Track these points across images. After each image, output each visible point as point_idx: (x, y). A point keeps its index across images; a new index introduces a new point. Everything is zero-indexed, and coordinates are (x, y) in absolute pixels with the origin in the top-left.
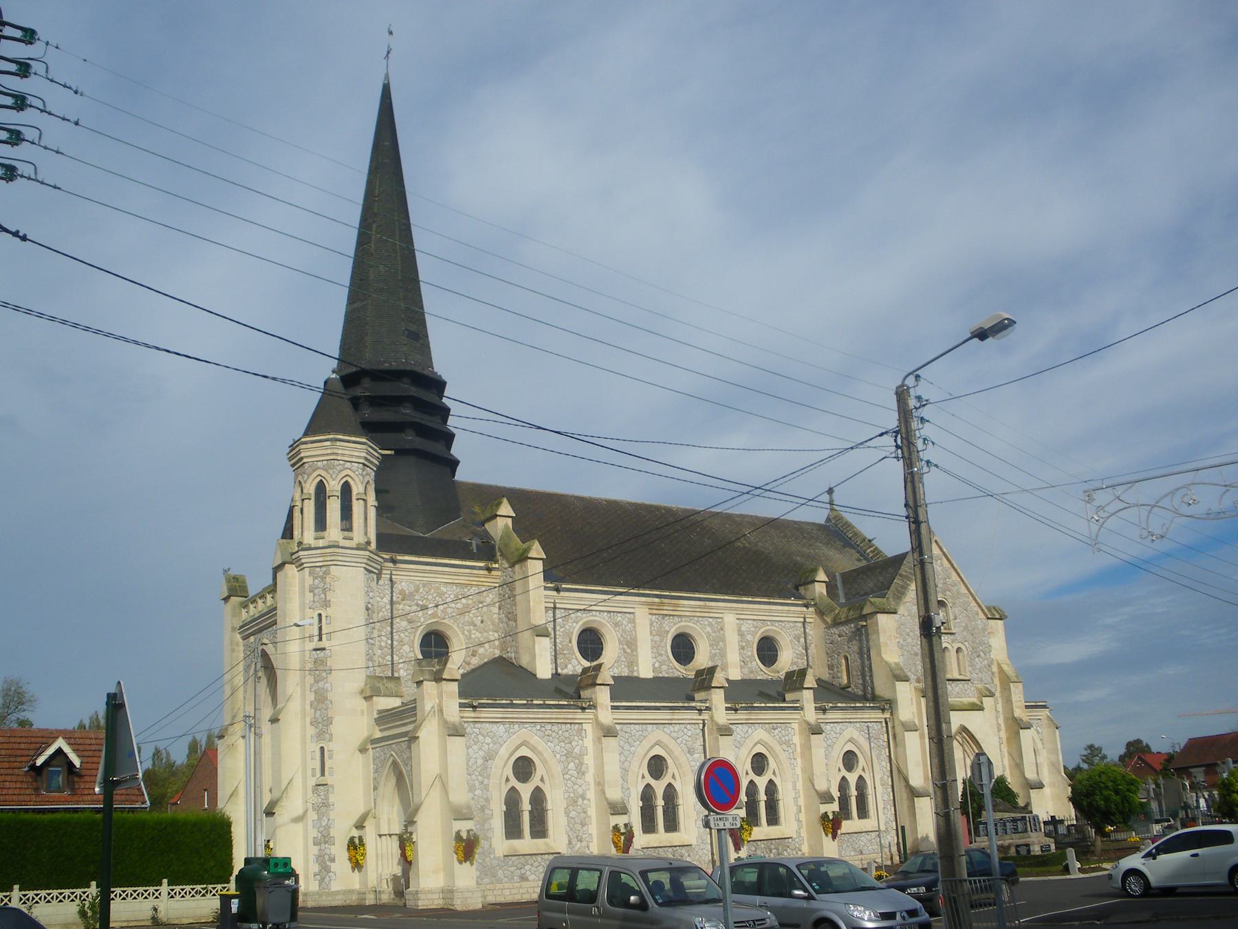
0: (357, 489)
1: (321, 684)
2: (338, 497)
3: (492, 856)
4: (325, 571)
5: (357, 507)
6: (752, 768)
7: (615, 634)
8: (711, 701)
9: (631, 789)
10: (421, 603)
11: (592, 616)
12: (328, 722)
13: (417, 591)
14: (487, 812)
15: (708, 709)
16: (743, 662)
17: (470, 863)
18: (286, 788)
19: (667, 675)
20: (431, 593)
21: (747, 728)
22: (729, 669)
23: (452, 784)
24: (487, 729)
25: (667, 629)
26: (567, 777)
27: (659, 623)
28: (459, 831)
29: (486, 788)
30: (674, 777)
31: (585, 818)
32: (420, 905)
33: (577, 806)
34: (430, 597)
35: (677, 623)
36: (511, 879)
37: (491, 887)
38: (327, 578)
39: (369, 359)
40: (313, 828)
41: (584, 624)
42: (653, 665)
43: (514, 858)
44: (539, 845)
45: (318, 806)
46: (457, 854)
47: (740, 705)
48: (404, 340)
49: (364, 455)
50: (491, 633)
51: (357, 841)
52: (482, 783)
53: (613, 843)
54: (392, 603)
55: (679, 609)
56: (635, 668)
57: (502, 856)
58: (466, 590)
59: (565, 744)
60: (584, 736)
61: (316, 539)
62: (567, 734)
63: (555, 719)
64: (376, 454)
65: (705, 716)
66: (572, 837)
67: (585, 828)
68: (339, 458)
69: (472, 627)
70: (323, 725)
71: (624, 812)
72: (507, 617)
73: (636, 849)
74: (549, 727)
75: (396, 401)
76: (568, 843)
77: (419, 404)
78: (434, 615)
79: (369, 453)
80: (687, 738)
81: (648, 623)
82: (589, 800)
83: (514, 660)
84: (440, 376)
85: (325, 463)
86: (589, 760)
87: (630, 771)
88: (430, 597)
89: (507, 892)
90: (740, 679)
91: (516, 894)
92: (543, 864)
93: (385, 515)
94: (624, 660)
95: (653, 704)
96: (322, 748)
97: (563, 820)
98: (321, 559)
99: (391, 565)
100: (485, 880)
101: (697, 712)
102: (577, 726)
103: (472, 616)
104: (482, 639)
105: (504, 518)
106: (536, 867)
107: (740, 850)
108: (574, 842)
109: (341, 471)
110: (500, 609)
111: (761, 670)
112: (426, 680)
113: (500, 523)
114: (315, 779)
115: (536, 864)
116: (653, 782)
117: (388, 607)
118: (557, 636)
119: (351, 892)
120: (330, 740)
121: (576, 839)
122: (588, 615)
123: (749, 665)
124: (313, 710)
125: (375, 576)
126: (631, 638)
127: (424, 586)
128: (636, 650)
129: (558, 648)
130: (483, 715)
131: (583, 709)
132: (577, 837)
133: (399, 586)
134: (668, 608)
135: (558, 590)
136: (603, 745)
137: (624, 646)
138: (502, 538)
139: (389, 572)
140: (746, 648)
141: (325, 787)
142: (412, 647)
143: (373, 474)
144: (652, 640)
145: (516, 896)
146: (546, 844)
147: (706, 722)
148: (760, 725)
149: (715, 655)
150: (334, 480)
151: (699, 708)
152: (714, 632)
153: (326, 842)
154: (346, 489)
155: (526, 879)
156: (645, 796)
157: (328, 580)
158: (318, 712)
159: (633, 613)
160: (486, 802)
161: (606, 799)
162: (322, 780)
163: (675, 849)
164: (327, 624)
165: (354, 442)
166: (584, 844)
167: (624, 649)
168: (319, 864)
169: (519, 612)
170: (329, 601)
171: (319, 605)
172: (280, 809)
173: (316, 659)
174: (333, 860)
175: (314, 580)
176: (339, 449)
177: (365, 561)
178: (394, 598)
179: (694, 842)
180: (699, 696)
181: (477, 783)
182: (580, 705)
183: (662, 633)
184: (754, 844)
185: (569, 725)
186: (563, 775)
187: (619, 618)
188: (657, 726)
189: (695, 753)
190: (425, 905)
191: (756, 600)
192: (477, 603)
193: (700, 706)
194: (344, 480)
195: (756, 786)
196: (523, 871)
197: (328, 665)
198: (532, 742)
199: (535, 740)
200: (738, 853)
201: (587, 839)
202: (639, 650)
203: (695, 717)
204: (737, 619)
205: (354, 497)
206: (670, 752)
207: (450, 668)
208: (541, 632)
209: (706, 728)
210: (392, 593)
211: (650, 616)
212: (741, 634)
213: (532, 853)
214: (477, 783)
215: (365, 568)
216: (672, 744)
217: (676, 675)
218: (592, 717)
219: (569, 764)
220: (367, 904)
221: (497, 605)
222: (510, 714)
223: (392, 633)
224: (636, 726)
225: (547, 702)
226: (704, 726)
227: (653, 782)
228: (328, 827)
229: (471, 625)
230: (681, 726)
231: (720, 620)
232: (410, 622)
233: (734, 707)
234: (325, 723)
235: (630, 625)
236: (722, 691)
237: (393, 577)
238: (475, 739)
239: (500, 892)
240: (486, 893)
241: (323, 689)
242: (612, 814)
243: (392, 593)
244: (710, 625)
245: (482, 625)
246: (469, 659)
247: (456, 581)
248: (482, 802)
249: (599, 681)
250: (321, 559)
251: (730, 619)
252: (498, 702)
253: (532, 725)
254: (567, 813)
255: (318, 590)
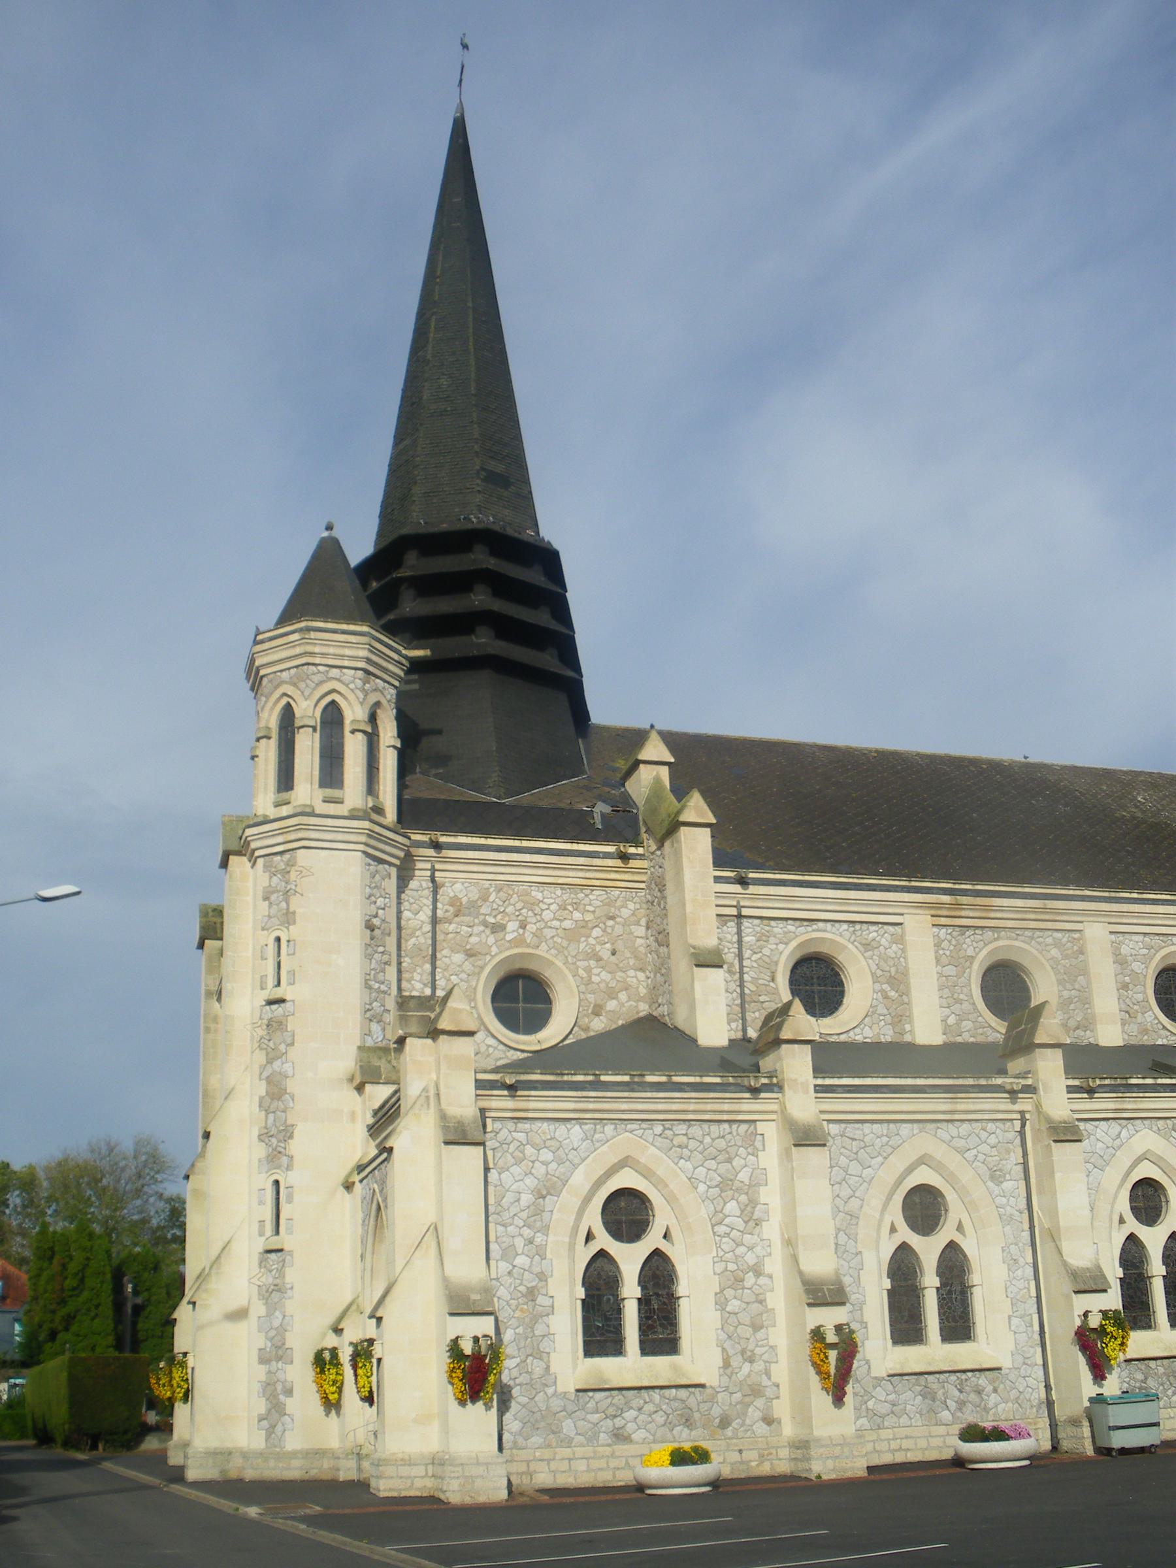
0: (354, 712)
1: (277, 1064)
2: (314, 729)
3: (550, 1391)
4: (289, 860)
5: (354, 748)
6: (1132, 1209)
7: (865, 963)
8: (1036, 1073)
9: (866, 1254)
10: (492, 920)
11: (818, 930)
12: (287, 1133)
13: (485, 899)
14: (540, 1300)
15: (1031, 1089)
16: (1127, 1012)
17: (485, 1404)
18: (219, 1257)
19: (972, 1040)
20: (512, 901)
21: (1118, 1128)
22: (1099, 1026)
23: (452, 1243)
24: (544, 1133)
25: (970, 952)
26: (721, 1229)
27: (954, 942)
28: (457, 1338)
29: (541, 1253)
30: (960, 1228)
31: (761, 1314)
32: (382, 1488)
33: (743, 1288)
34: (510, 909)
35: (990, 943)
36: (592, 1439)
37: (547, 1454)
38: (291, 873)
39: (419, 521)
40: (259, 1331)
41: (801, 945)
42: (944, 1021)
43: (599, 1396)
44: (660, 1367)
45: (267, 1291)
46: (452, 1384)
47: (1098, 1082)
48: (478, 484)
49: (364, 653)
50: (631, 973)
51: (327, 1355)
52: (531, 1242)
53: (812, 1365)
54: (435, 921)
55: (993, 915)
56: (908, 1027)
57: (573, 1390)
58: (581, 895)
59: (718, 1163)
60: (761, 1148)
61: (277, 805)
62: (721, 1144)
63: (694, 1111)
64: (396, 657)
65: (1025, 1104)
66: (731, 1352)
67: (761, 1334)
68: (317, 661)
69: (592, 963)
70: (279, 1141)
71: (837, 1300)
72: (657, 941)
73: (876, 1378)
74: (681, 1128)
75: (461, 583)
76: (721, 1364)
77: (502, 586)
78: (519, 941)
79: (372, 650)
80: (984, 1148)
81: (930, 941)
82: (771, 1277)
83: (667, 1018)
84: (549, 543)
85: (293, 671)
86: (771, 1196)
87: (861, 1217)
88: (510, 909)
89: (581, 1466)
90: (1121, 1044)
91: (601, 1469)
92: (664, 1407)
93: (434, 771)
94: (885, 1012)
95: (909, 1081)
96: (277, 1182)
97: (713, 1318)
98: (280, 839)
99: (431, 852)
100: (533, 1440)
101: (1006, 1095)
102: (744, 1127)
103: (593, 942)
104: (613, 984)
105: (654, 766)
106: (650, 1415)
107: (1103, 1378)
108: (735, 1362)
109: (321, 683)
110: (648, 928)
111: (1164, 1027)
112: (411, 1035)
113: (645, 775)
114: (263, 1239)
115: (650, 1407)
116: (915, 1241)
117: (427, 927)
118: (745, 970)
119: (320, 1453)
120: (289, 1168)
121: (740, 1358)
122: (810, 929)
123: (1140, 1018)
124: (263, 1112)
125: (394, 871)
126: (897, 972)
127: (499, 889)
128: (907, 993)
129: (747, 991)
130: (532, 1105)
131: (755, 1091)
132: (743, 1352)
133: (450, 890)
134: (971, 914)
135: (743, 882)
136: (794, 1164)
137: (885, 986)
138: (648, 801)
139: (429, 866)
140: (1131, 986)
141: (279, 1254)
142: (472, 999)
143: (393, 692)
144: (940, 975)
145: (599, 1473)
146: (675, 1368)
147: (1028, 1116)
148: (1146, 1122)
149: (1069, 1001)
150: (306, 700)
151: (1008, 1087)
152: (1066, 957)
153: (279, 1359)
154: (332, 718)
155: (627, 1439)
156: (899, 1268)
157: (293, 875)
158: (271, 1116)
159: (901, 924)
160: (541, 1280)
161: (801, 1273)
162: (275, 1243)
163: (963, 1376)
164: (288, 955)
165: (344, 632)
166: (759, 1366)
167: (882, 991)
168: (268, 1399)
169: (672, 930)
170: (294, 913)
171: (279, 923)
172: (204, 1296)
173: (270, 1020)
174: (289, 1392)
175: (271, 878)
176: (329, 645)
177: (363, 839)
178: (440, 913)
179: (1006, 1362)
180: (1016, 1065)
181: (519, 1243)
182: (746, 1083)
183: (960, 961)
184: (1141, 1365)
185: (726, 1126)
186: (713, 1226)
187: (872, 933)
188: (921, 1125)
189: (1005, 1180)
190: (393, 1490)
191: (1145, 896)
192: (603, 919)
193: (1011, 1083)
194: (328, 699)
195: (1144, 1247)
196: (619, 1422)
197: (289, 1030)
198: (643, 1160)
199: (651, 1154)
200: (1101, 1386)
201: (765, 1357)
202: (914, 993)
203: (1002, 1107)
204: (1111, 932)
205: (348, 727)
206: (951, 1179)
207: (456, 1010)
208: (708, 960)
209: (1028, 1128)
210: (435, 901)
211: (935, 930)
212: (1121, 961)
213: (639, 1384)
214: (519, 1243)
215: (364, 852)
216: (953, 1162)
217: (990, 1039)
218: (775, 1107)
219: (725, 1203)
220: (341, 1480)
221: (643, 922)
222: (592, 1102)
223: (433, 974)
224: (875, 1126)
225: (676, 1079)
226: (1023, 1126)
227: (915, 1241)
228: (282, 1330)
229: (590, 959)
230: (975, 1125)
231: (1077, 936)
232: (470, 954)
233: (1085, 1085)
234: (281, 1136)
235: (894, 947)
236: (1059, 1053)
237: (437, 874)
238: (517, 1153)
239: (564, 1466)
240: (532, 1466)
241: (280, 1073)
242: (809, 1305)
243: (435, 901)
244: (1057, 944)
245: (613, 958)
246: (587, 1020)
247: (561, 881)
248: (530, 1281)
249: (785, 1034)
250: (280, 839)
251: (1096, 933)
252: (566, 1078)
253: (644, 1125)
254: (721, 1303)
255: (275, 895)
